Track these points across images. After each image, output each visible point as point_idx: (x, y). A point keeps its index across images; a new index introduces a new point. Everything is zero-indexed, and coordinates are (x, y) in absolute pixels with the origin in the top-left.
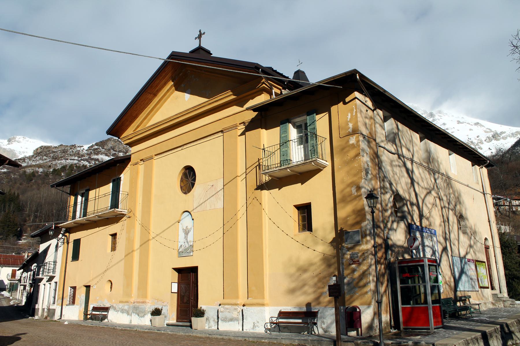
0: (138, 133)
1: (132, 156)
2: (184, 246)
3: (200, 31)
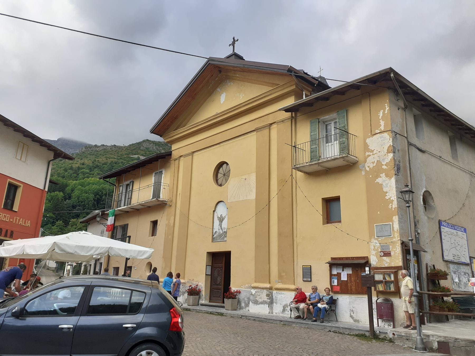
0: (178, 132)
1: (172, 152)
2: (218, 232)
3: (234, 39)
